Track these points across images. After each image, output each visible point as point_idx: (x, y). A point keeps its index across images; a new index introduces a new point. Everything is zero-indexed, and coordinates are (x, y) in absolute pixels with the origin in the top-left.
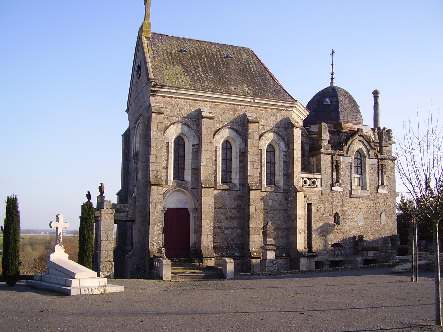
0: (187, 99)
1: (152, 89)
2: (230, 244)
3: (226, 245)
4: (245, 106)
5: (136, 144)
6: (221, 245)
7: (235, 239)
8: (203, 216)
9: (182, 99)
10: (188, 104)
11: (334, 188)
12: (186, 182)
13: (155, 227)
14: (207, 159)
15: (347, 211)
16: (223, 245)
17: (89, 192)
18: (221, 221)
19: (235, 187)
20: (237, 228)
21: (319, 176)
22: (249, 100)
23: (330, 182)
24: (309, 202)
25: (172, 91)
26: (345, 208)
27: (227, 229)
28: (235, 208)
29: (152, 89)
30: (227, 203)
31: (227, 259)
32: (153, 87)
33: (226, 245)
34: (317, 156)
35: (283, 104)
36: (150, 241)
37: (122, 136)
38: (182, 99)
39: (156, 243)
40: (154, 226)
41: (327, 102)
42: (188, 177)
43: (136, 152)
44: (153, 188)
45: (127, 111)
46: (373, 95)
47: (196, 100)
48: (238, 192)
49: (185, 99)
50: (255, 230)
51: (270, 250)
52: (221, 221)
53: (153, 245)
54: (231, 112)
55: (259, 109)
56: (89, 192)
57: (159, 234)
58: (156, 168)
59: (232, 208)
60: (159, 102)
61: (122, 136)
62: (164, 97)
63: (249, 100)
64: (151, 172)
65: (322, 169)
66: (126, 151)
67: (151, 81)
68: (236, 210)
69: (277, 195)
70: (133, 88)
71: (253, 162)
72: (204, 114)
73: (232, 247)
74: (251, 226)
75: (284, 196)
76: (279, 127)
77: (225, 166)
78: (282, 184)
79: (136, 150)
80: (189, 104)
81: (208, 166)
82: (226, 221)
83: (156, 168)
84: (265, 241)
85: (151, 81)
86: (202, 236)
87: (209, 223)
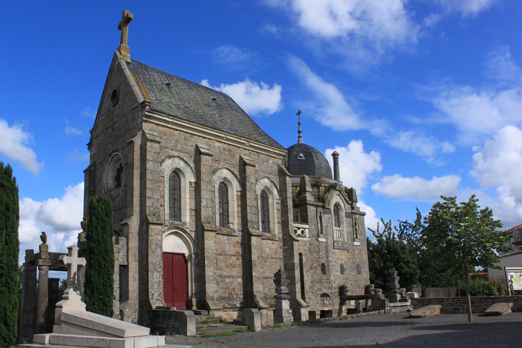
0: (182, 131)
1: (146, 113)
2: (232, 294)
3: (227, 295)
4: (239, 147)
5: (107, 180)
6: (223, 295)
7: (236, 288)
8: (206, 262)
9: (177, 130)
10: (183, 137)
11: (320, 239)
12: (185, 224)
13: (155, 273)
14: (207, 199)
15: (331, 261)
16: (225, 296)
17: (43, 233)
18: (221, 268)
19: (234, 232)
20: (238, 277)
21: (307, 226)
22: (244, 142)
23: (315, 233)
24: (300, 252)
25: (168, 119)
26: (329, 259)
27: (227, 278)
28: (234, 256)
29: (146, 113)
30: (226, 249)
31: (252, 309)
32: (147, 112)
33: (227, 295)
34: (302, 207)
35: (275, 151)
36: (150, 290)
37: (84, 171)
38: (177, 130)
39: (157, 292)
40: (154, 272)
41: (302, 157)
42: (187, 217)
43: (108, 190)
44: (152, 227)
45: (90, 145)
46: (332, 157)
47: (191, 134)
48: (237, 238)
49: (180, 131)
50: (258, 279)
51: (285, 299)
52: (221, 268)
53: (153, 294)
54: (226, 152)
55: (252, 153)
56: (43, 233)
57: (159, 281)
58: (153, 204)
59: (231, 255)
60: (154, 131)
61: (84, 171)
62: (158, 125)
63: (244, 142)
64: (147, 209)
65: (309, 220)
66: (91, 188)
67: (146, 103)
68: (235, 257)
69: (273, 243)
70: (101, 118)
71: (251, 207)
72: (202, 150)
73: (233, 297)
74: (254, 274)
75: (279, 244)
76: (271, 174)
77: (221, 210)
78: (277, 232)
79: (108, 188)
80: (185, 138)
81: (208, 207)
82: (226, 269)
83: (153, 204)
84: (278, 291)
85: (146, 103)
86: (207, 285)
87: (213, 270)
